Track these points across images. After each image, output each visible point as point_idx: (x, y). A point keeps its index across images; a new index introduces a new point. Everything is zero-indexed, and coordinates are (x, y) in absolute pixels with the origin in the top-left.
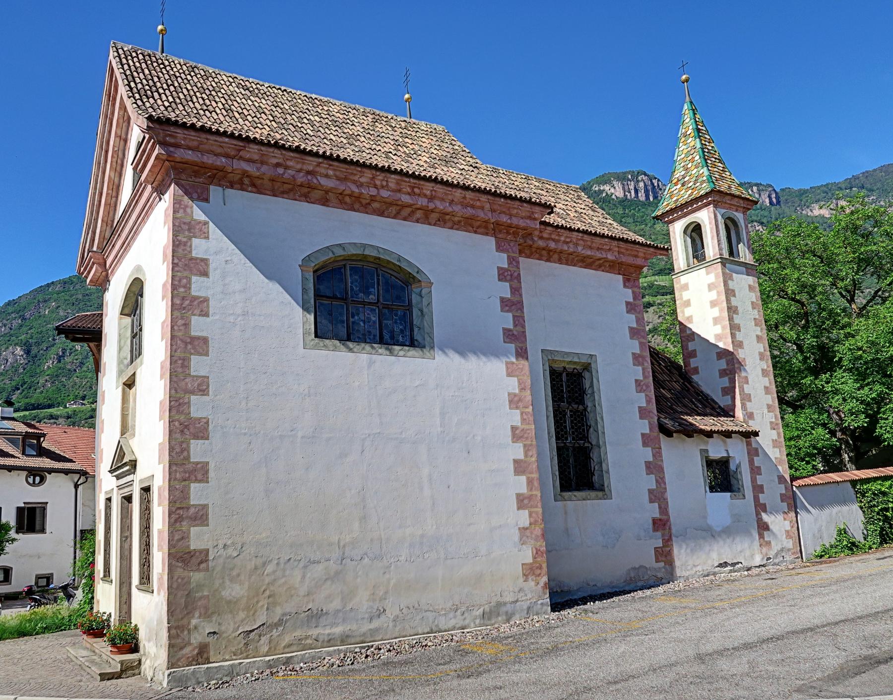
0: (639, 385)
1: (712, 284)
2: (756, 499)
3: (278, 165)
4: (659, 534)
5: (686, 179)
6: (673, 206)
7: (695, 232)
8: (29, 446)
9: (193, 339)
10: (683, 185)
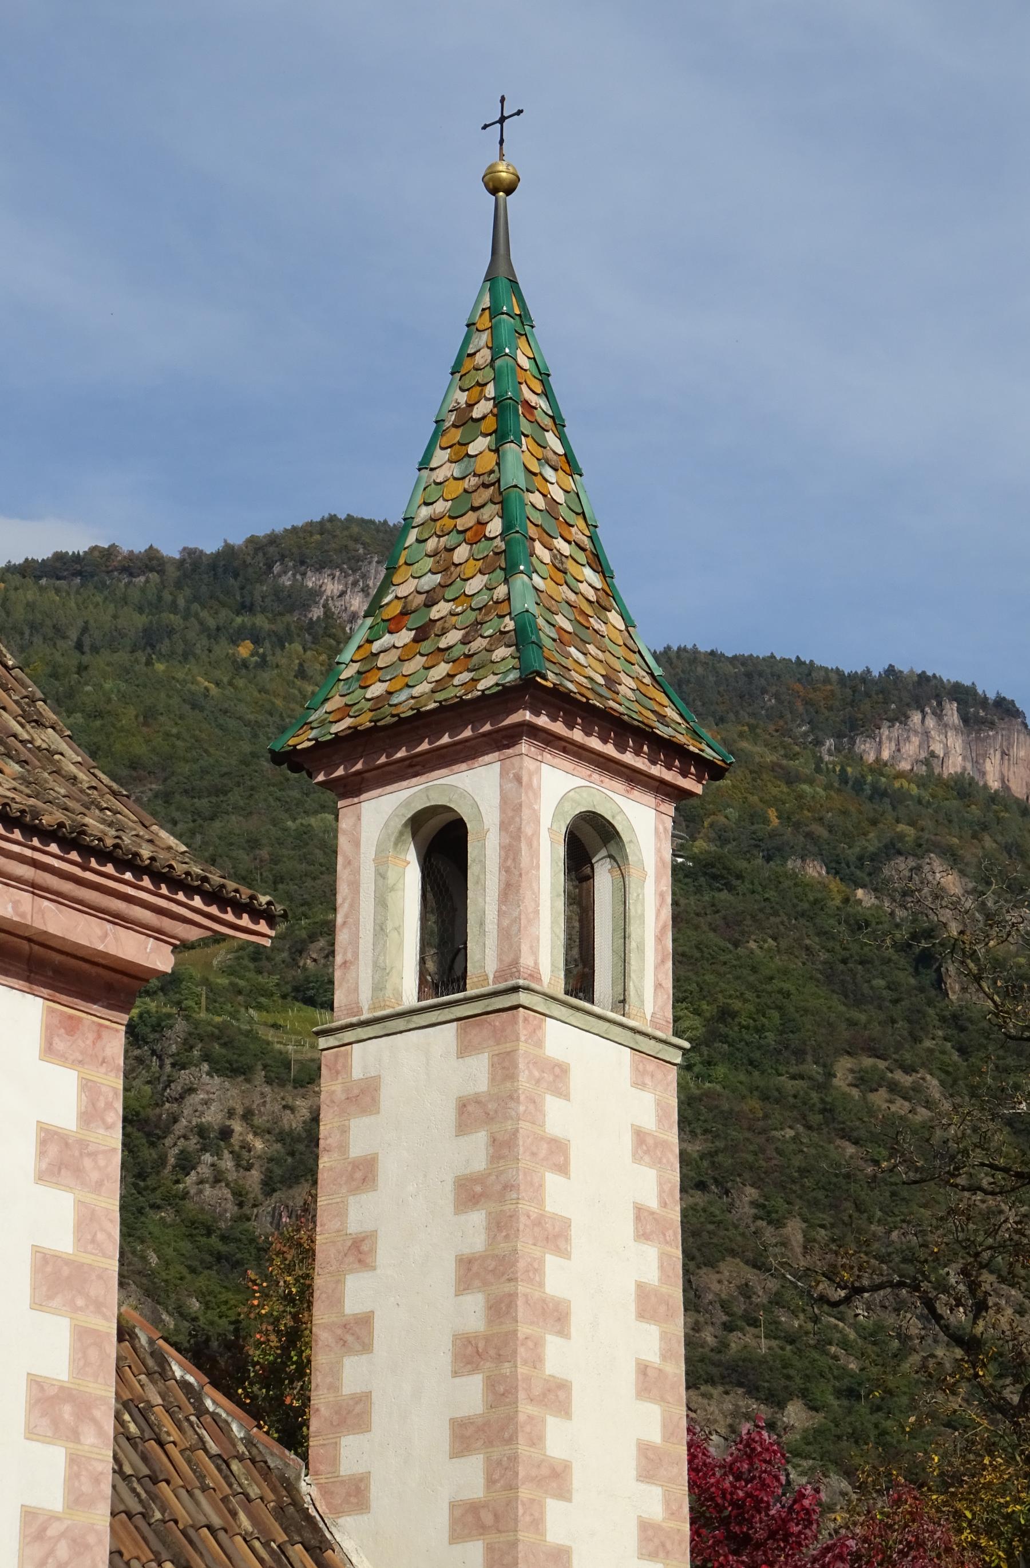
0: (40, 1536)
1: (477, 1100)
5: (435, 613)
6: (365, 721)
10: (422, 634)
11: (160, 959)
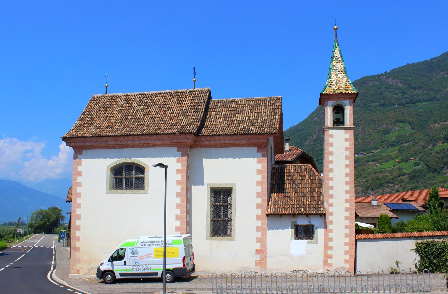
2: (326, 244)
3: (96, 141)
4: (259, 256)
8: (73, 249)
9: (78, 193)
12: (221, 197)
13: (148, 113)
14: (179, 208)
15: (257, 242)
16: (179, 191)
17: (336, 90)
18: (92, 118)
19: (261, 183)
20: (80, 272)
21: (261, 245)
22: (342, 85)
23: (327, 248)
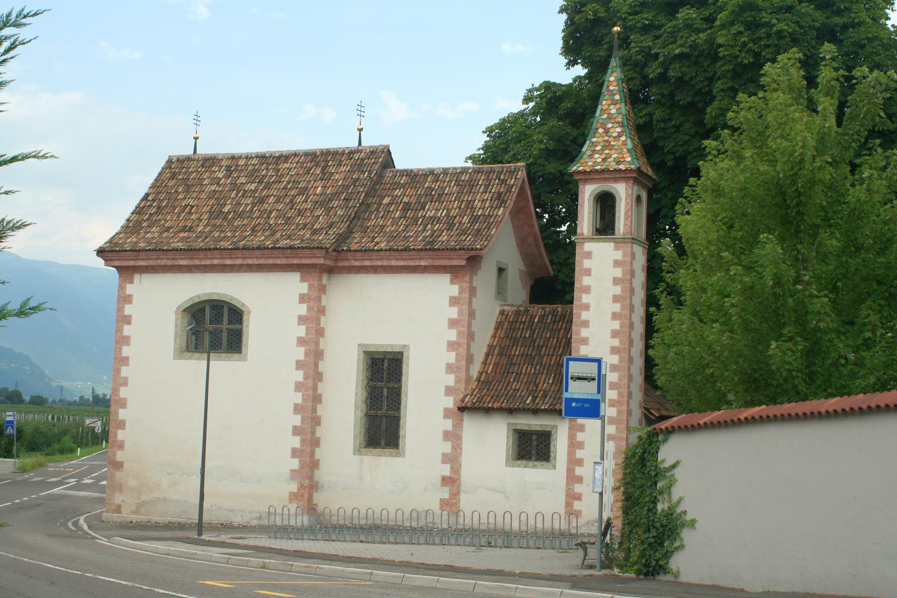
4: (447, 489)
7: (606, 202)
9: (123, 358)
11: (463, 263)
12: (384, 374)
13: (262, 201)
14: (300, 391)
15: (444, 462)
16: (301, 357)
17: (598, 164)
18: (159, 207)
19: (456, 346)
20: (123, 509)
21: (452, 468)
22: (613, 151)
23: (573, 478)
